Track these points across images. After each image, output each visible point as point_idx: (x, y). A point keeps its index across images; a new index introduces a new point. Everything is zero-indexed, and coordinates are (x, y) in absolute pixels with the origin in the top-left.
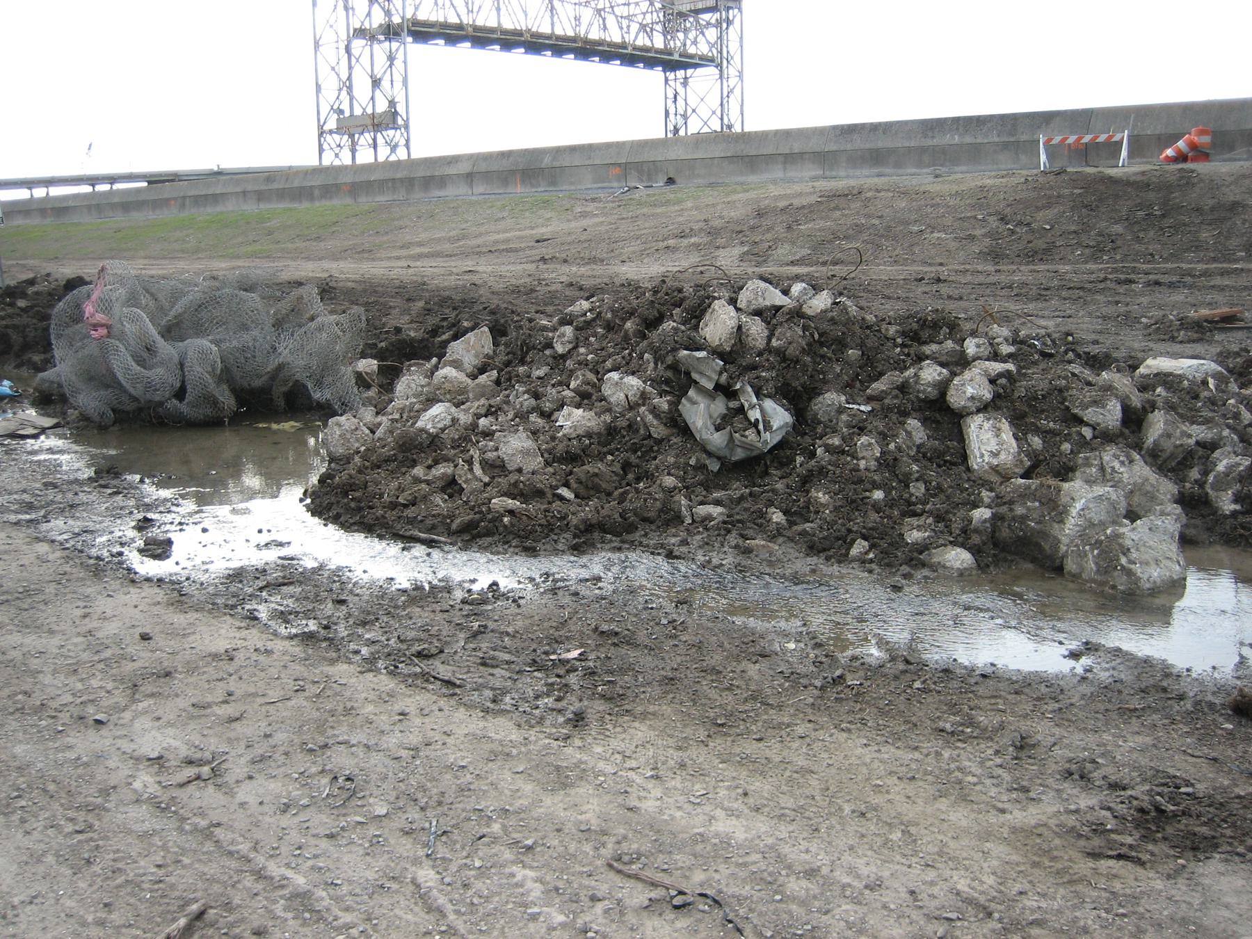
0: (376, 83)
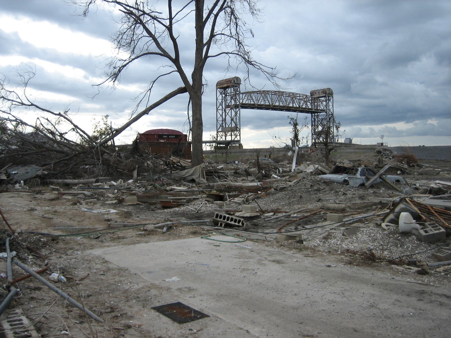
0: (232, 120)
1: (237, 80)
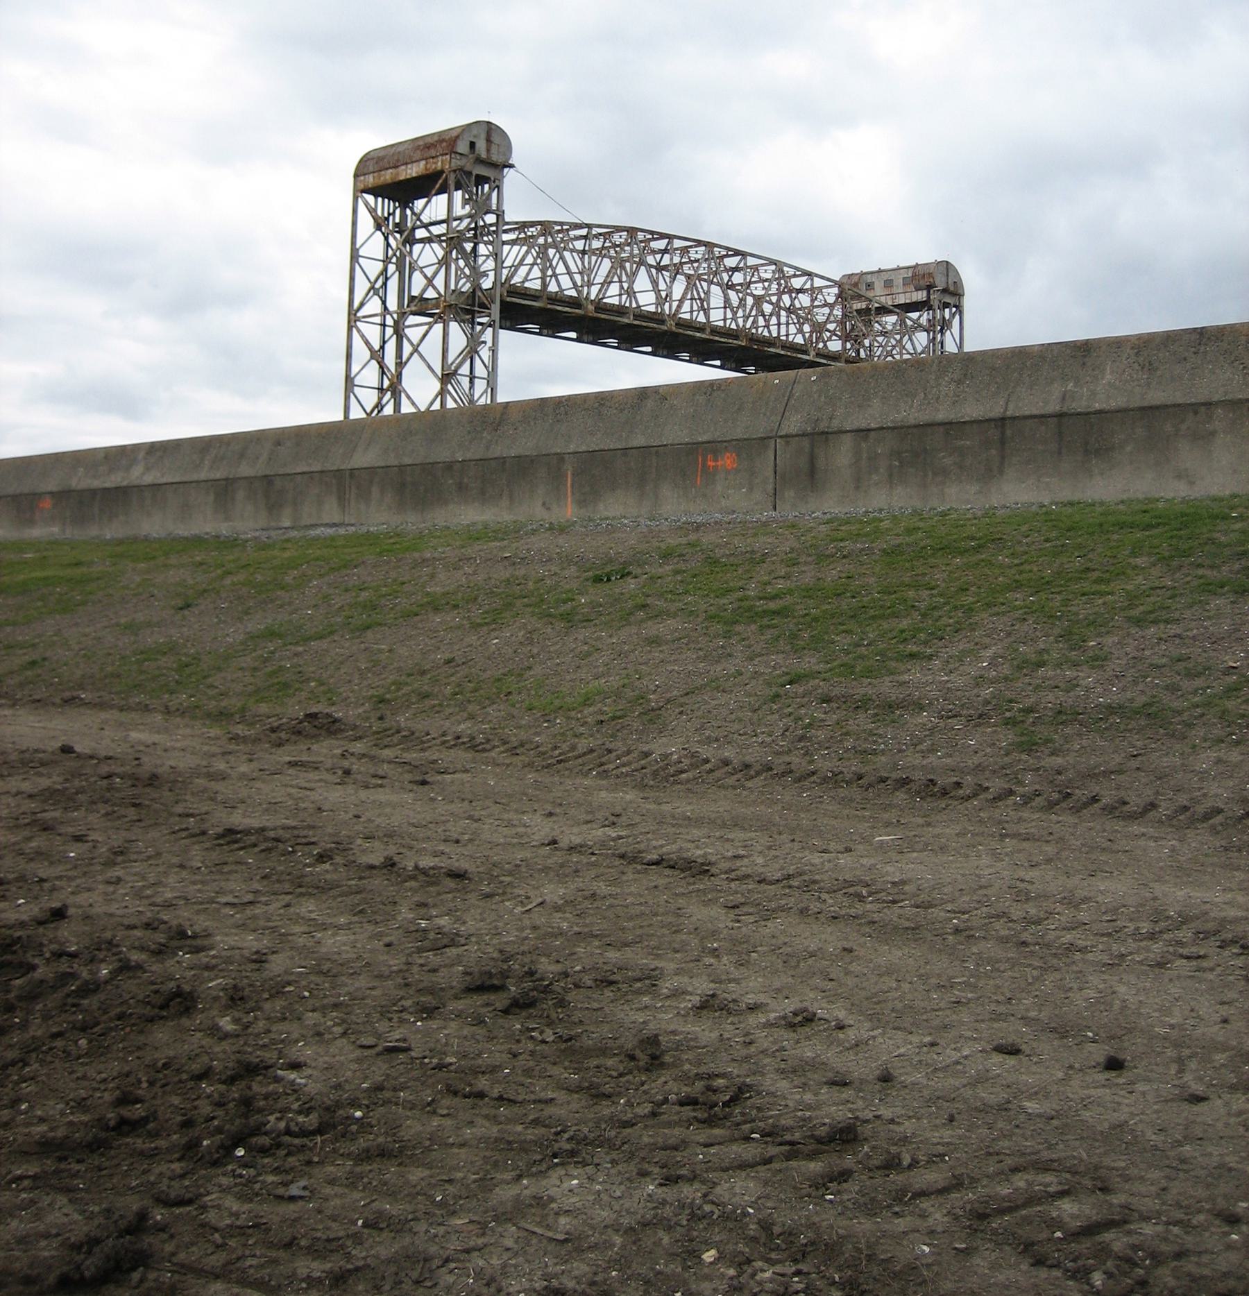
1: (489, 140)
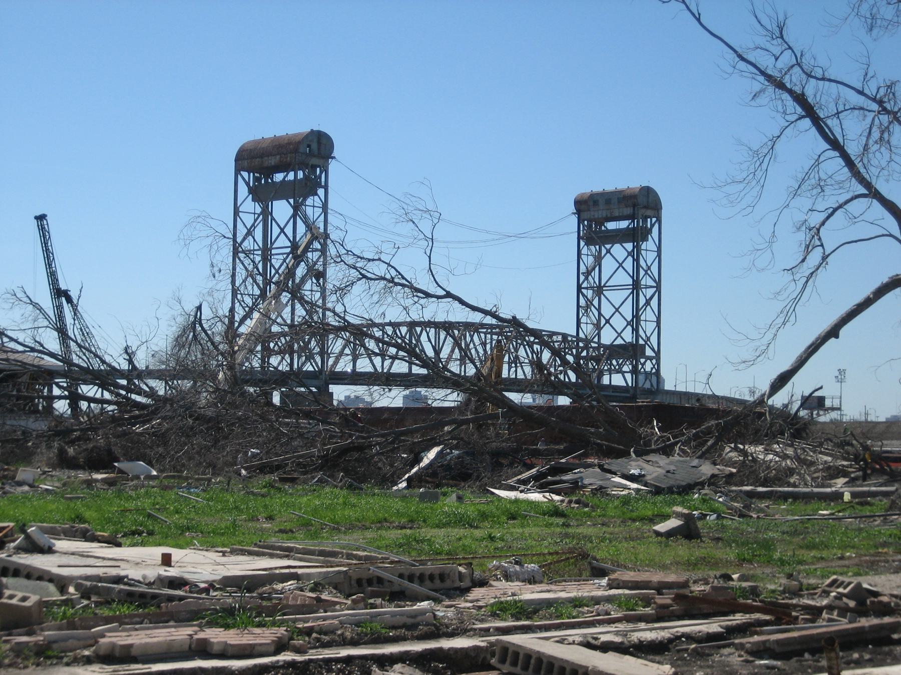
1: (319, 143)
